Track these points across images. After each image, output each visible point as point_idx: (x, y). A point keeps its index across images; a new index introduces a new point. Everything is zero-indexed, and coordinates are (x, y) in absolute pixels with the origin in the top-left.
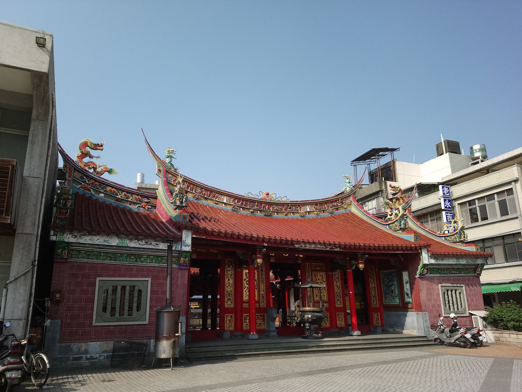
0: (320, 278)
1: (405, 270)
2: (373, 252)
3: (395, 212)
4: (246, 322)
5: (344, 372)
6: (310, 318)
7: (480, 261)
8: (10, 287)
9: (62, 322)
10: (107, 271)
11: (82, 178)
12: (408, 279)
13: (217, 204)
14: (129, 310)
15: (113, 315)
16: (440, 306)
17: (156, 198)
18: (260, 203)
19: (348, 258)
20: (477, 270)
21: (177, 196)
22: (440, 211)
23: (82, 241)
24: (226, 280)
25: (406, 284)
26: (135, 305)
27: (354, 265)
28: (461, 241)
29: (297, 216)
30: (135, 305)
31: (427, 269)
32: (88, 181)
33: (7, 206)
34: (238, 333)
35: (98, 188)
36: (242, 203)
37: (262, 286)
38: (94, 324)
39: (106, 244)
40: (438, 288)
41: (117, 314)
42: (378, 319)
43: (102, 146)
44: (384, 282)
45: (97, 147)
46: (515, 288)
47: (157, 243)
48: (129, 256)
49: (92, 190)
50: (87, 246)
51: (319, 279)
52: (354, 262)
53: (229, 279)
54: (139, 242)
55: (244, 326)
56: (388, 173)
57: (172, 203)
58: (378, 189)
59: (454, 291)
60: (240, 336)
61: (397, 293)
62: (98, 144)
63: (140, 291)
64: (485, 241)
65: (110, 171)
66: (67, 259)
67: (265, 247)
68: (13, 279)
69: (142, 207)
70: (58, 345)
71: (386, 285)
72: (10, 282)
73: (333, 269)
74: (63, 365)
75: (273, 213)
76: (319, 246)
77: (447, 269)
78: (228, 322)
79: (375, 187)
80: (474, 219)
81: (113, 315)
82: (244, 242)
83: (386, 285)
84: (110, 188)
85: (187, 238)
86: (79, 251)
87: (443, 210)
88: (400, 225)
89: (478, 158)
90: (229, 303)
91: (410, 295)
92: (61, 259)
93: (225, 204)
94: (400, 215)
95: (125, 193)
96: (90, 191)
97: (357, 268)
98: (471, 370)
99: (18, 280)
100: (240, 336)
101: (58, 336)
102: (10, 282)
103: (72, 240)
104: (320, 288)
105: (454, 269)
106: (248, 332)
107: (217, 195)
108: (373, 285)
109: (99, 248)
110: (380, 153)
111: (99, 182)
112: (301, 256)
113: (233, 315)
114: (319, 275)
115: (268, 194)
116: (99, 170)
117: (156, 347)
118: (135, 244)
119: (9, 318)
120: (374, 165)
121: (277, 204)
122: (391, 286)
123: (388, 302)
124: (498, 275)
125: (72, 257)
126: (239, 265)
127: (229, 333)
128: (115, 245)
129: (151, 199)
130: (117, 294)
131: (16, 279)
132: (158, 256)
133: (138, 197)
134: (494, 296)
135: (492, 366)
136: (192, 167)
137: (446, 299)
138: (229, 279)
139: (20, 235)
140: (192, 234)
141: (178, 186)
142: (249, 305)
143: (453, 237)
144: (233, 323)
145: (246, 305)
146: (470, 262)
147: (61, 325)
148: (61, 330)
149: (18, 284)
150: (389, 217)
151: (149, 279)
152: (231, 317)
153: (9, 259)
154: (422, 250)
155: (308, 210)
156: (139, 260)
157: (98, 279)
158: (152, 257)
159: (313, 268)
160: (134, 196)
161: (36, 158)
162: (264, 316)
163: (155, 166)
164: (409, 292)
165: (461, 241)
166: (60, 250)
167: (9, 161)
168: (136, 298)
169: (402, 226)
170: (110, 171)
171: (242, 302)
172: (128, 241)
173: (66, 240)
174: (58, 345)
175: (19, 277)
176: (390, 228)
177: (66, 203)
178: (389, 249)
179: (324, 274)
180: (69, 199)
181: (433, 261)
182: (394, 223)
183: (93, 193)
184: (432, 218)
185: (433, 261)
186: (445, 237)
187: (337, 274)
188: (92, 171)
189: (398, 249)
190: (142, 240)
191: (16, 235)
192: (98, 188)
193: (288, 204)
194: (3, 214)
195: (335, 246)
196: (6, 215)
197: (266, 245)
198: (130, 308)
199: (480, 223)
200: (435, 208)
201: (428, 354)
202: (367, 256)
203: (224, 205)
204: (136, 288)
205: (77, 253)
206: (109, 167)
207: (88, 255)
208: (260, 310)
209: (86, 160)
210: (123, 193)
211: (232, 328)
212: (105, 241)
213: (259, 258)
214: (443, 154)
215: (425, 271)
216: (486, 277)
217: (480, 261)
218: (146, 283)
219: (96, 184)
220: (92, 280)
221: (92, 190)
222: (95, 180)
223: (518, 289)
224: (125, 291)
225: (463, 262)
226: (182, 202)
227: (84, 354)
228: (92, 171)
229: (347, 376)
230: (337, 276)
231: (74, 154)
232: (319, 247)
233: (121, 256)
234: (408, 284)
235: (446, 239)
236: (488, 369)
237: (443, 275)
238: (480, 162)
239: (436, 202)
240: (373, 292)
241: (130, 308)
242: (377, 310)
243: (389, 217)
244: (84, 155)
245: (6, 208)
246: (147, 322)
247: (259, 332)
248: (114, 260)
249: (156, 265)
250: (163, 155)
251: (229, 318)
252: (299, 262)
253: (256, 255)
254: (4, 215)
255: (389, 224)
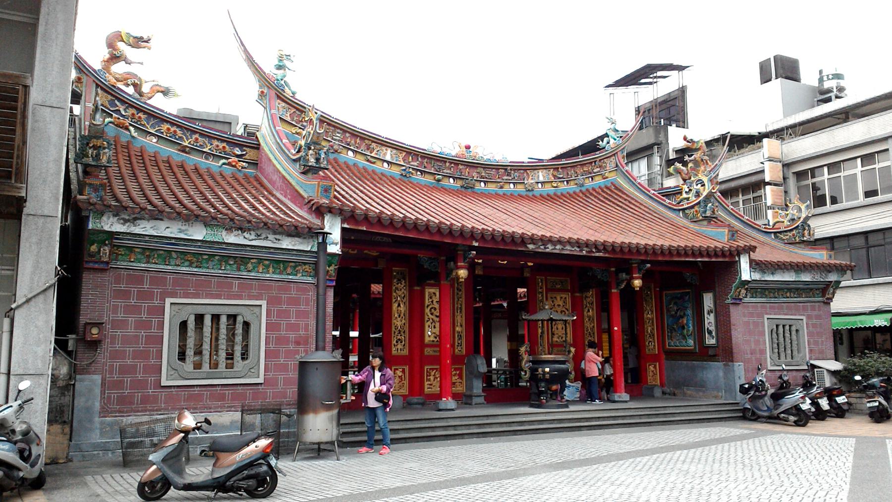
0: (561, 303)
1: (708, 290)
2: (660, 259)
3: (695, 187)
4: (429, 380)
5: (621, 462)
6: (548, 373)
7: (832, 277)
8: (19, 316)
9: (103, 380)
10: (182, 286)
11: (112, 103)
12: (712, 306)
13: (374, 163)
14: (227, 359)
15: (198, 366)
16: (763, 352)
17: (257, 147)
18: (455, 162)
19: (613, 269)
20: (826, 291)
21: (310, 149)
22: (760, 184)
23: (137, 230)
24: (395, 306)
25: (708, 313)
26: (238, 349)
27: (623, 281)
28: (706, 218)
29: (520, 189)
30: (238, 349)
31: (746, 289)
32: (125, 110)
33: (17, 163)
34: (415, 399)
35: (143, 125)
36: (422, 163)
37: (459, 318)
38: (164, 383)
39: (182, 236)
40: (763, 323)
41: (206, 367)
42: (655, 374)
43: (765, 78)
44: (668, 311)
45: (139, 42)
46: (880, 321)
47: (278, 237)
48: (225, 259)
49: (132, 129)
50: (147, 238)
51: (559, 305)
52: (624, 276)
53: (399, 305)
54: (245, 234)
55: (426, 386)
56: (672, 109)
57: (295, 161)
58: (652, 141)
59: (787, 328)
60: (419, 404)
61: (691, 328)
62: (142, 38)
63: (246, 325)
64: (837, 244)
65: (166, 92)
66: (107, 263)
67: (474, 248)
68: (24, 300)
69: (229, 164)
70: (97, 419)
71: (672, 316)
72: (18, 307)
73: (584, 288)
74: (110, 455)
75: (477, 184)
76: (568, 247)
77: (779, 289)
78: (651, 374)
79: (647, 137)
80: (820, 201)
81: (198, 366)
82: (437, 238)
83: (672, 316)
84: (168, 126)
85: (334, 229)
86: (131, 249)
87: (769, 184)
88: (705, 212)
89: (829, 91)
90: (399, 347)
91: (714, 334)
92: (96, 262)
93: (389, 163)
94: (705, 194)
95: (197, 136)
96: (130, 131)
97: (629, 285)
98: (827, 458)
99: (32, 303)
100: (419, 404)
101: (97, 405)
102: (18, 307)
103: (118, 227)
104: (566, 321)
105: (790, 290)
106: (439, 397)
107: (374, 145)
108: (649, 315)
109: (168, 244)
110: (660, 73)
111: (145, 113)
112: (530, 264)
113: (407, 368)
114: (559, 298)
115: (468, 147)
116: (145, 89)
117: (299, 424)
118: (237, 238)
119: (21, 372)
120: (646, 94)
121: (486, 166)
122: (682, 317)
123: (674, 343)
124: (860, 301)
125: (117, 260)
126: (420, 277)
127: (402, 398)
128: (200, 238)
129: (248, 149)
130: (205, 329)
131: (28, 301)
132: (278, 262)
133: (221, 145)
134: (842, 335)
135: (855, 450)
136: (326, 93)
137: (775, 341)
138: (399, 305)
139: (31, 217)
140: (343, 222)
141: (309, 129)
142: (440, 351)
143: (790, 234)
144: (406, 382)
145: (428, 351)
146: (818, 278)
147: (103, 384)
148: (103, 393)
149: (33, 309)
150: (684, 195)
151: (264, 303)
152: (403, 371)
153: (14, 262)
154: (742, 256)
155: (541, 179)
156: (242, 267)
157: (168, 301)
158: (267, 262)
159: (549, 287)
160: (216, 143)
161: (56, 69)
162: (461, 370)
163: (253, 87)
164: (712, 328)
165: (706, 218)
166: (94, 248)
167: (18, 77)
168: (241, 337)
169: (708, 214)
170: (166, 92)
171: (423, 345)
172: (224, 233)
173: (106, 228)
174: (97, 419)
175: (34, 296)
176: (686, 216)
177: (98, 155)
178: (679, 254)
179: (568, 296)
180: (104, 148)
181: (757, 276)
182: (692, 207)
183: (135, 135)
184: (746, 197)
185: (757, 276)
186: (775, 233)
187: (591, 296)
188: (130, 90)
189: (701, 255)
190: (249, 230)
191: (23, 217)
192: (143, 125)
193: (504, 167)
194: (11, 178)
195: (596, 248)
196: (16, 181)
197: (476, 244)
198: (230, 356)
199: (829, 207)
200: (753, 179)
201: (746, 432)
202: (649, 265)
203: (385, 165)
204: (240, 319)
205: (127, 252)
206: (165, 84)
207: (148, 257)
208: (457, 360)
209: (119, 68)
210: (194, 137)
211: (405, 391)
212: (181, 231)
213: (462, 268)
214: (770, 80)
215: (743, 291)
216: (842, 302)
217: (832, 277)
218: (256, 310)
219: (140, 117)
220: (156, 302)
221: (132, 129)
222: (139, 110)
223: (886, 324)
224: (218, 324)
225: (806, 277)
226: (318, 160)
227: (147, 436)
228: (130, 90)
229: (630, 469)
230: (588, 300)
231: (95, 58)
232: (568, 250)
233: (208, 260)
234: (712, 315)
235: (776, 237)
236: (852, 455)
237: (773, 300)
238: (833, 98)
239: (756, 167)
240: (650, 328)
241: (230, 356)
242: (654, 358)
243: (684, 195)
244: (115, 58)
245: (17, 169)
246: (261, 380)
247: (456, 397)
248: (196, 267)
249: (276, 277)
250: (269, 67)
251: (652, 368)
252: (527, 274)
253: (456, 262)
254: (13, 181)
255: (684, 210)
